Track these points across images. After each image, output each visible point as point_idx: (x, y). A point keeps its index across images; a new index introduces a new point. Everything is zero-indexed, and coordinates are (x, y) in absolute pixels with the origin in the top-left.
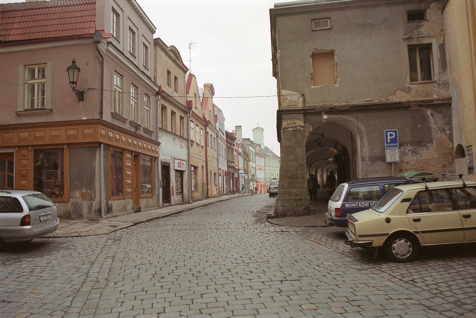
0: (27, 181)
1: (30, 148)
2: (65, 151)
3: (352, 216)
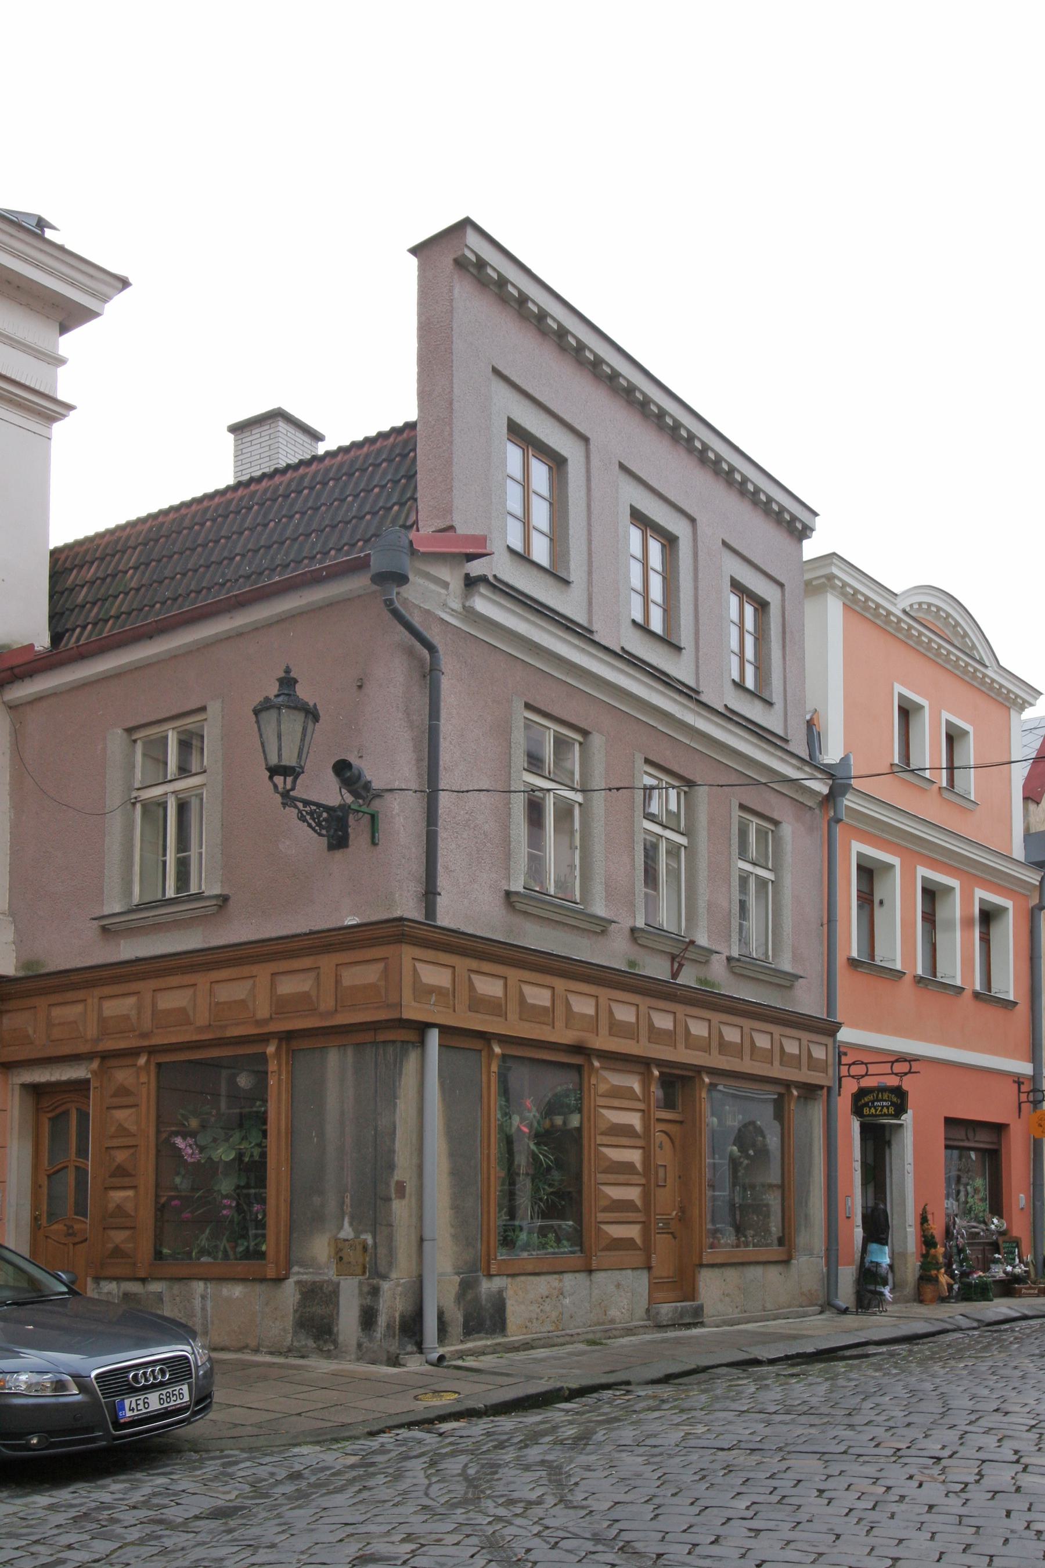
0: (130, 1193)
1: (142, 1061)
2: (273, 1066)
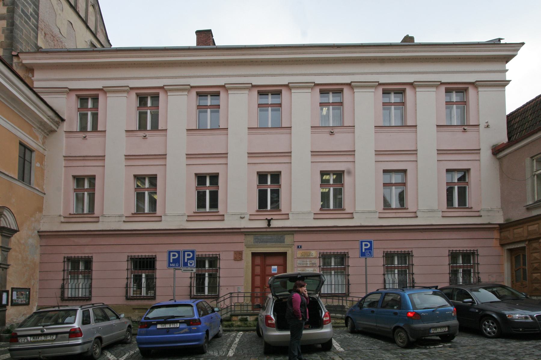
3: (75, 5)
